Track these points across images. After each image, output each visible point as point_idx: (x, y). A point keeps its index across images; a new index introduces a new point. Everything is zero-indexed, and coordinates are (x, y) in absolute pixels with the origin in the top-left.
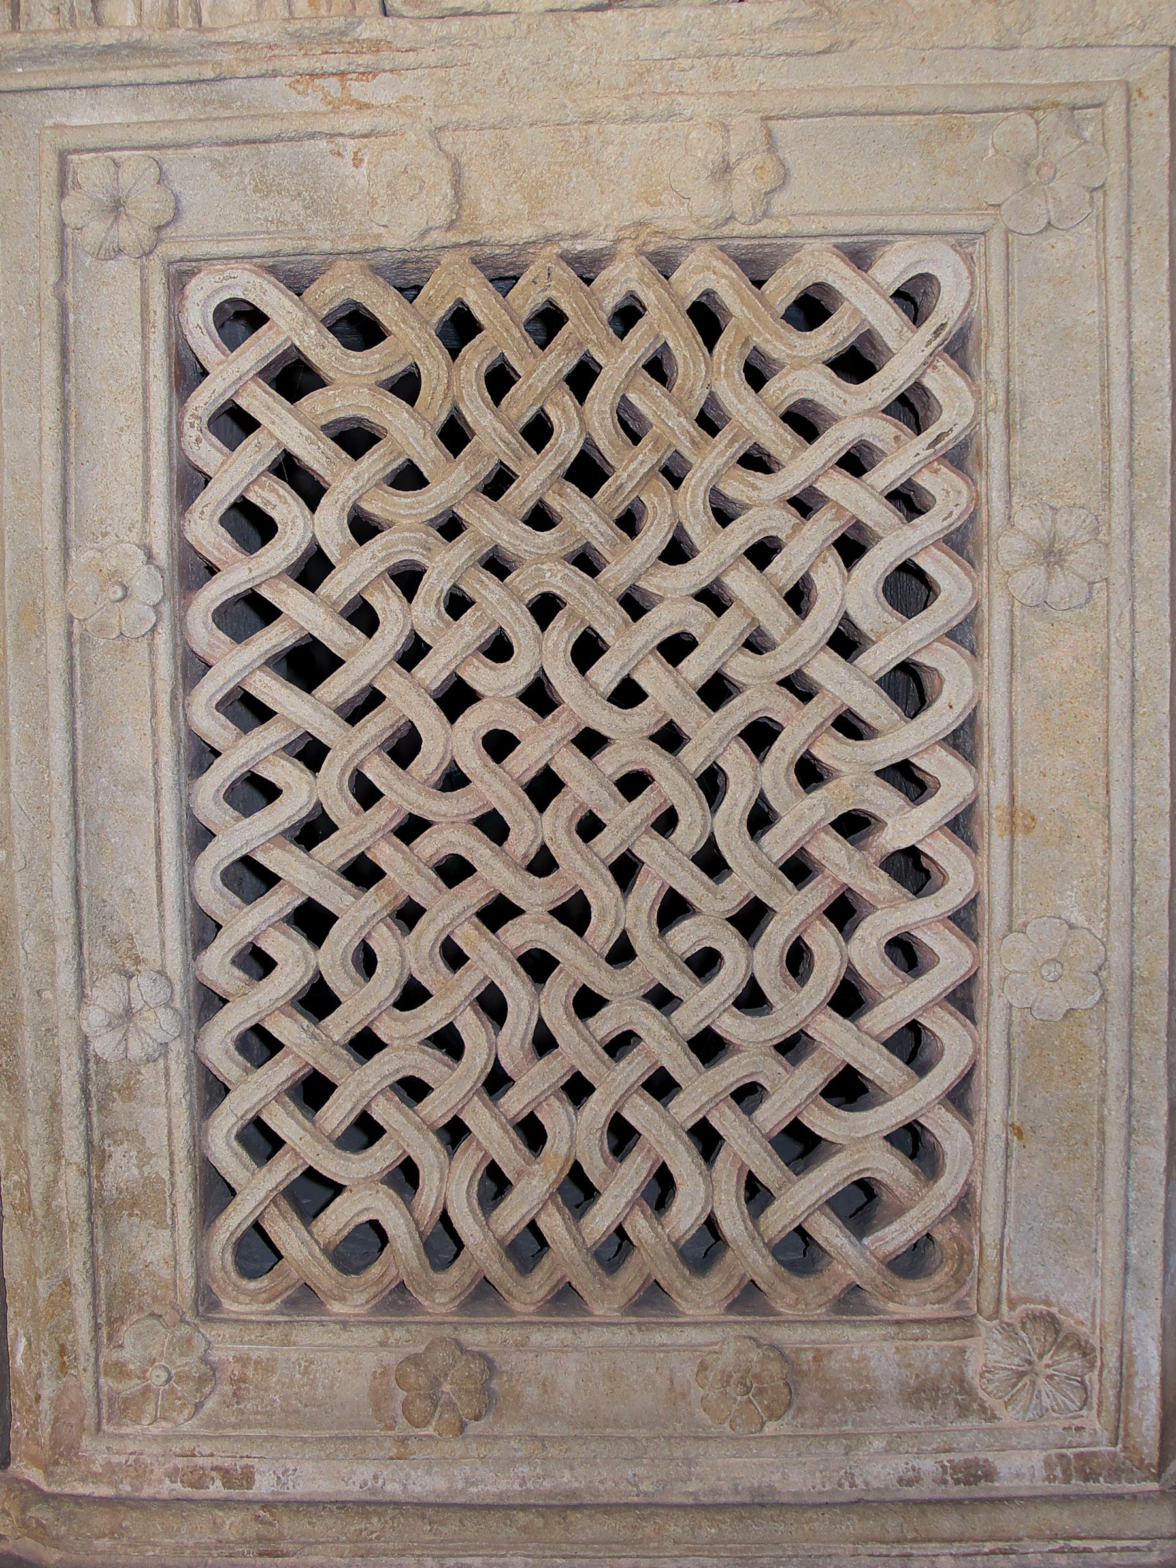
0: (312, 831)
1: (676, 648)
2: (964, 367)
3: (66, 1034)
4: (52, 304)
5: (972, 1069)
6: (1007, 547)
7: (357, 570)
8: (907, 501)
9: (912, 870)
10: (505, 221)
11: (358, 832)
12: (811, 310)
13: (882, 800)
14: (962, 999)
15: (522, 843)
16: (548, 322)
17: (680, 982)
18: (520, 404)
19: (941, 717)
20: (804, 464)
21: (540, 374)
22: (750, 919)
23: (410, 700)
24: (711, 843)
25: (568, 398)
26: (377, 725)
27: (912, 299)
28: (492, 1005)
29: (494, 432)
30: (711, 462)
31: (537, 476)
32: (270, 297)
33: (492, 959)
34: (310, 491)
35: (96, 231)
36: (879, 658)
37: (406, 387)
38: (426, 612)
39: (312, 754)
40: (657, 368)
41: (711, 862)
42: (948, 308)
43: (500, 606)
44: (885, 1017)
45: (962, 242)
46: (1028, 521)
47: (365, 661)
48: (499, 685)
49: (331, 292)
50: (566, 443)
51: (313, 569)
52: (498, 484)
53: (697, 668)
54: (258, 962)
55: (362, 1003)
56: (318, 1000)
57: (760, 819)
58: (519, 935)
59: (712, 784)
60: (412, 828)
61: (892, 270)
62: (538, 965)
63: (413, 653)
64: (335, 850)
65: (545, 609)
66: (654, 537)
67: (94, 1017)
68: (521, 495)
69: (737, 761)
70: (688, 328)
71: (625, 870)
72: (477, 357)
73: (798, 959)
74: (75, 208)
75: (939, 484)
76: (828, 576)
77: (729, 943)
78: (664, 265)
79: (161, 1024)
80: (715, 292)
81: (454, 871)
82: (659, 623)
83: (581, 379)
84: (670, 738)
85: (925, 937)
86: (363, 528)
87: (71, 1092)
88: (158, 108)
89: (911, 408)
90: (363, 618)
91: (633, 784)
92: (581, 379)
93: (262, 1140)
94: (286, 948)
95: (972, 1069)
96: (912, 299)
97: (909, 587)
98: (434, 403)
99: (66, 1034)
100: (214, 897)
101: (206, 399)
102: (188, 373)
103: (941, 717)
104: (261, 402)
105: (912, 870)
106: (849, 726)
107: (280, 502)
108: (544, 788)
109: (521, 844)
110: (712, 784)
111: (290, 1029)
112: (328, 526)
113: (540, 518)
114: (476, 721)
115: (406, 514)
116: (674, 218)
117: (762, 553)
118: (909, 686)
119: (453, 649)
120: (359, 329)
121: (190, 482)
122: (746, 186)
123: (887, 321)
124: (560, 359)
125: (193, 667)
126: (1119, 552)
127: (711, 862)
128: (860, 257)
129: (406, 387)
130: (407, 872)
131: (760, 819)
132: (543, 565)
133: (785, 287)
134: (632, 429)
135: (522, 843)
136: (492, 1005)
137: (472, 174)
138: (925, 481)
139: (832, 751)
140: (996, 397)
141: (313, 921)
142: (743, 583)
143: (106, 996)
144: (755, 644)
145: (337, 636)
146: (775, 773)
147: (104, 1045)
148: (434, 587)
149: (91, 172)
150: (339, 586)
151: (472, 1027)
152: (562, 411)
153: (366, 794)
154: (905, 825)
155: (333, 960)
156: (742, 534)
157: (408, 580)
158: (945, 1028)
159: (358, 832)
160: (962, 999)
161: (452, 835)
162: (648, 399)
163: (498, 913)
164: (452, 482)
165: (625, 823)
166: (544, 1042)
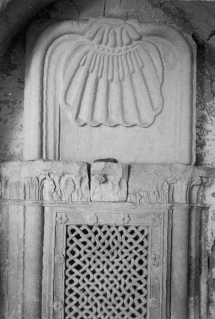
0: (78, 286)
1: (117, 267)
2: (147, 239)
3: (51, 308)
4: (54, 230)
5: (81, 184)
6: (149, 258)
7: (84, 258)
8: (141, 253)
9: (140, 292)
10: (102, 222)
11: (83, 286)
12: (132, 232)
13: (137, 284)
14: (145, 305)
15: (100, 288)
16: (105, 233)
17: (116, 303)
18: (102, 241)
19: (144, 276)
20: (131, 248)
21: (104, 238)
22: (124, 296)
23: (89, 272)
24: (120, 288)
25: (107, 240)
26: (85, 274)
27: (142, 232)
28: (96, 305)
29: (99, 244)
30: (121, 248)
31: (103, 248)
32: (76, 228)
33: (96, 300)
34: (79, 249)
35: (60, 221)
36: (138, 269)
37: (90, 239)
38: (91, 263)
39: (78, 277)
40: (116, 238)
41: (120, 290)
42: (146, 233)
43: (99, 262)
44: (137, 308)
45: (148, 227)
46: (153, 256)
47: (85, 267)
48: (98, 271)
49: (82, 228)
50: (107, 245)
51: (79, 257)
52: (99, 249)
53: (119, 270)
54: (71, 300)
55: (82, 305)
56: (77, 304)
57: (125, 286)
58: (99, 298)
59: (120, 282)
60: (89, 286)
61: (140, 229)
62: (101, 301)
63: (90, 267)
64: (80, 288)
65: (104, 262)
66: (115, 256)
67: (54, 306)
68: (101, 250)
69: (123, 280)
70: (120, 234)
71: (111, 291)
72: (97, 236)
73: (129, 301)
74: (57, 219)
75: (144, 251)
76: (133, 260)
77: (121, 299)
78: (117, 227)
79: (61, 306)
80: (23, 109)
81: (93, 291)
82: (116, 265)
83: (108, 238)
84: (116, 277)
85: (142, 299)
86: (85, 253)
87: (52, 313)
88: (67, 209)
89: (142, 243)
90: (84, 262)
91: (112, 282)
92: (108, 238)
93: (71, 310)
94: (75, 299)
95: (81, 184)
96: (142, 232)
97: (141, 262)
98: (93, 240)
99: (51, 308)
100: (67, 293)
101: (69, 239)
102: (67, 236)
103: (144, 276)
104: (74, 239)
105: (140, 292)
106: (135, 276)
107: (76, 250)
108: (103, 282)
109: (100, 288)
110: (120, 282)
111: (74, 308)
112: (82, 252)
113: (104, 253)
114: (96, 275)
115: (89, 252)
116: (118, 224)
117: (126, 258)
118: (141, 272)
119: (94, 267)
120: (85, 232)
121: (67, 248)
122: (126, 220)
123: (140, 234)
124: (106, 236)
125: (66, 268)
126: (161, 260)
127: (120, 290)
128: (137, 228)
129: (90, 239)
130: (88, 291)
131: (125, 286)
132: (103, 258)
133: (129, 230)
134: (113, 244)
135: (100, 288)
136: (96, 305)
137: (99, 217)
138: (143, 251)
139: (132, 279)
140: (150, 242)
141: (77, 296)
142: (124, 261)
143: (56, 303)
144: (125, 267)
145: (81, 264)
146: (127, 281)
147: (55, 309)
148: (92, 260)
149: (59, 215)
150: (82, 259)
151: (94, 308)
152: (106, 242)
153: (84, 281)
154: (140, 287)
155: (80, 300)
156: (124, 255)
157: (89, 259)
158: (144, 309)
159: (83, 286)
160: (145, 305)
161: (93, 287)
162: (115, 241)
163: (97, 295)
164: (94, 249)
165: (111, 286)
166: (102, 309)
